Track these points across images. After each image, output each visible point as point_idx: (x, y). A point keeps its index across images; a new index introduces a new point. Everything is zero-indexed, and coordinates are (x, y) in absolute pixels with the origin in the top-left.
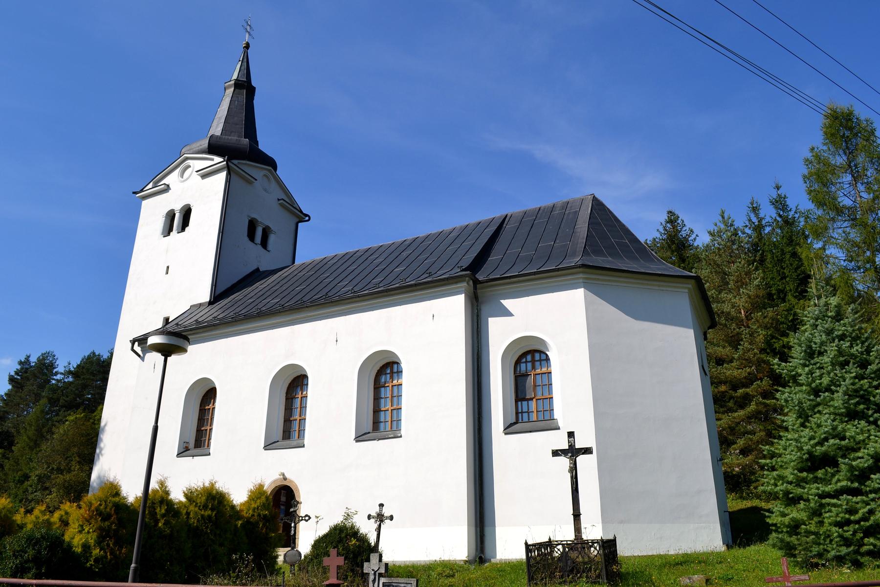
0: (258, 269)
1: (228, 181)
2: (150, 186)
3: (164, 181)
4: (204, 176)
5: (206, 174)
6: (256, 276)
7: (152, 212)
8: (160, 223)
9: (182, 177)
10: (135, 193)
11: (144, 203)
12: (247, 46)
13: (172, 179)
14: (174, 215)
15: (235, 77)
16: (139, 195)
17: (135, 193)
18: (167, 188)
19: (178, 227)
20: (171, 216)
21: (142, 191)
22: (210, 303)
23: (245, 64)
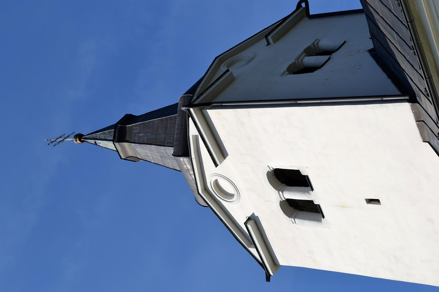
0: (372, 52)
1: (221, 105)
2: (253, 250)
3: (241, 221)
4: (223, 154)
5: (220, 152)
6: (382, 55)
7: (295, 244)
8: (304, 226)
9: (232, 196)
10: (268, 277)
11: (282, 262)
12: (80, 137)
13: (239, 212)
14: (288, 200)
15: (110, 145)
16: (269, 269)
17: (268, 277)
18: (253, 219)
19: (304, 192)
20: (294, 208)
21: (263, 265)
22: (413, 99)
23: (94, 135)
